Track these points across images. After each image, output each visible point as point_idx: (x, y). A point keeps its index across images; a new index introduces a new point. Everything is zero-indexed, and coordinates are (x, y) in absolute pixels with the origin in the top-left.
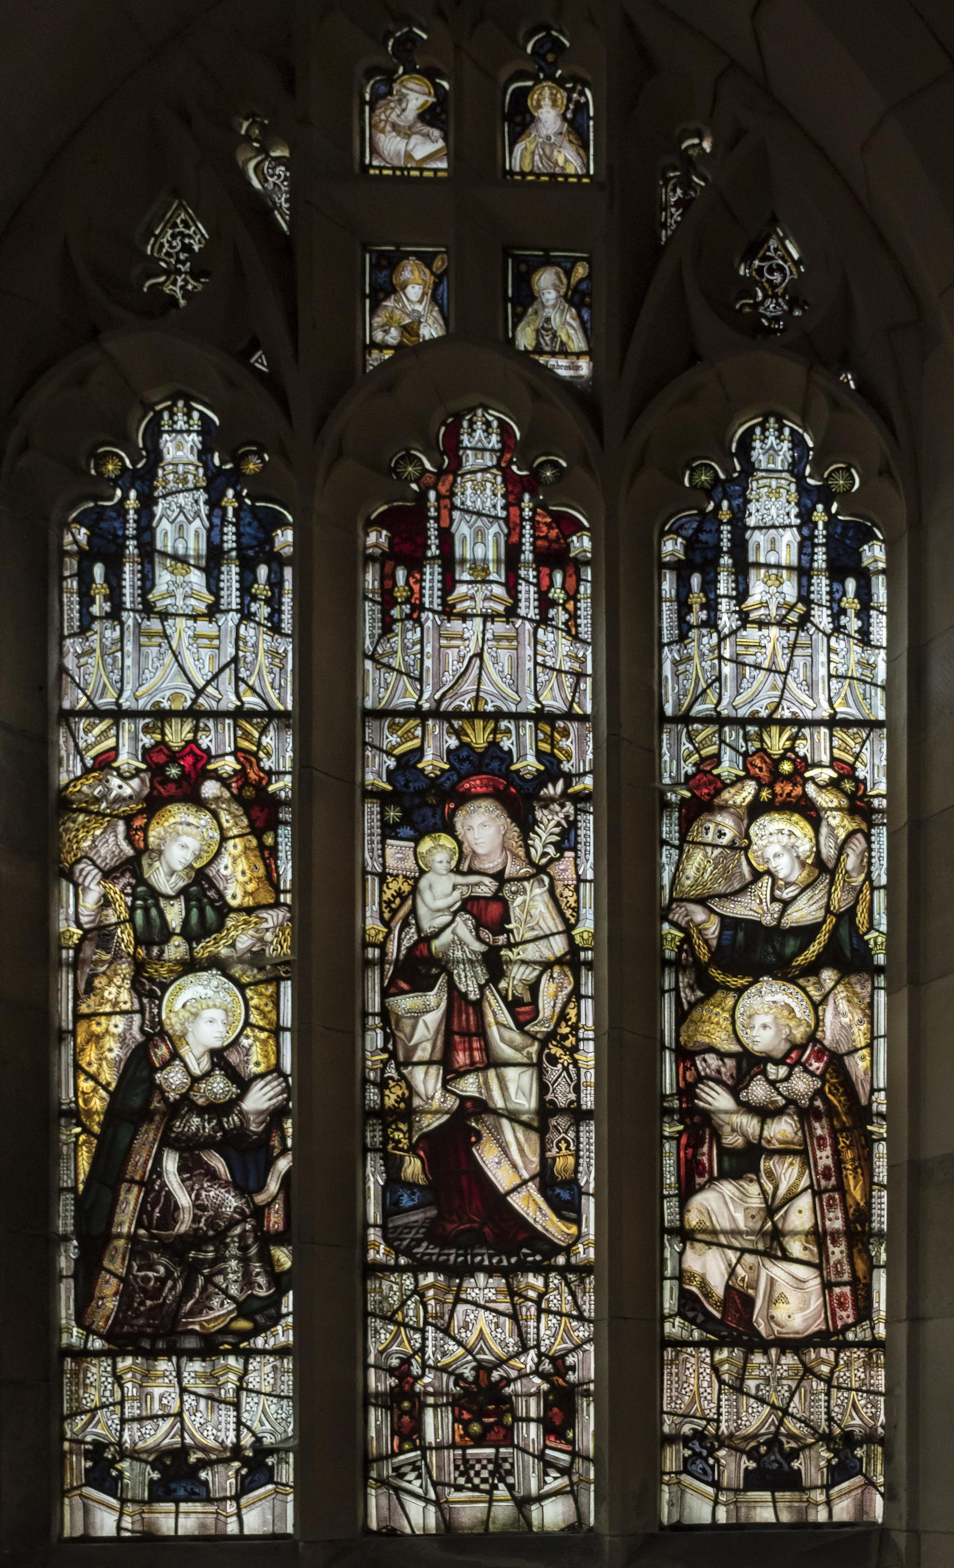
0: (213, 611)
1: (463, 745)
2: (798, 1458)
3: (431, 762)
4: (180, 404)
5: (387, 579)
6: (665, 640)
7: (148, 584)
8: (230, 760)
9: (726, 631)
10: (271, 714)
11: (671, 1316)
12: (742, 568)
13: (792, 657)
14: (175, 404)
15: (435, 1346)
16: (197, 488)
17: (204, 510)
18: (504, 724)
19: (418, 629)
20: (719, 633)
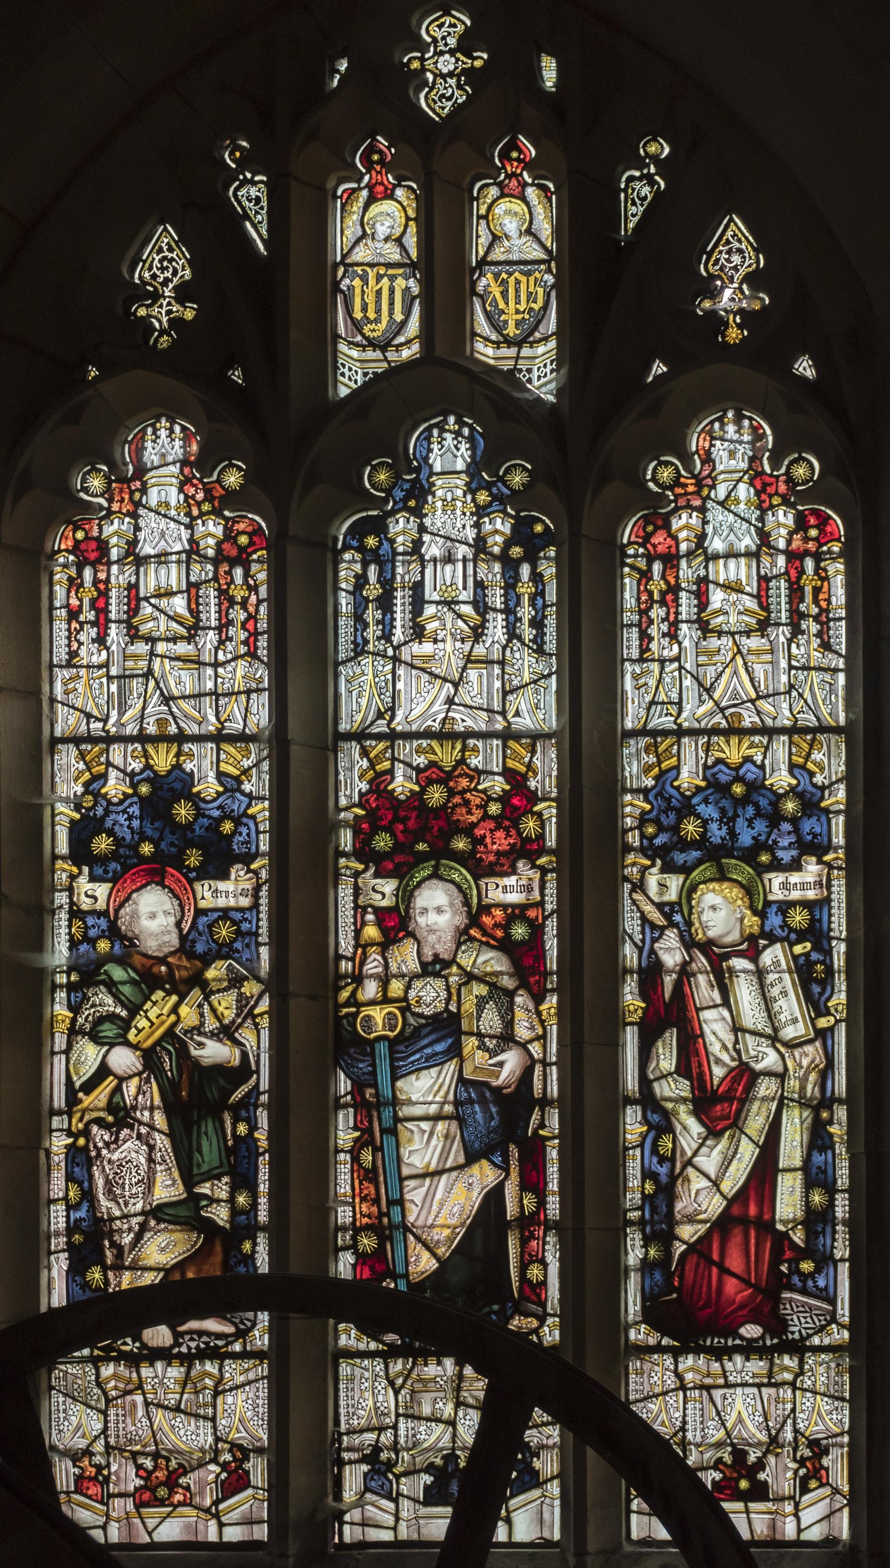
0: (763, 626)
4: (730, 414)
7: (704, 599)
10: (823, 729)
11: (636, 1323)
14: (724, 415)
18: (471, 742)
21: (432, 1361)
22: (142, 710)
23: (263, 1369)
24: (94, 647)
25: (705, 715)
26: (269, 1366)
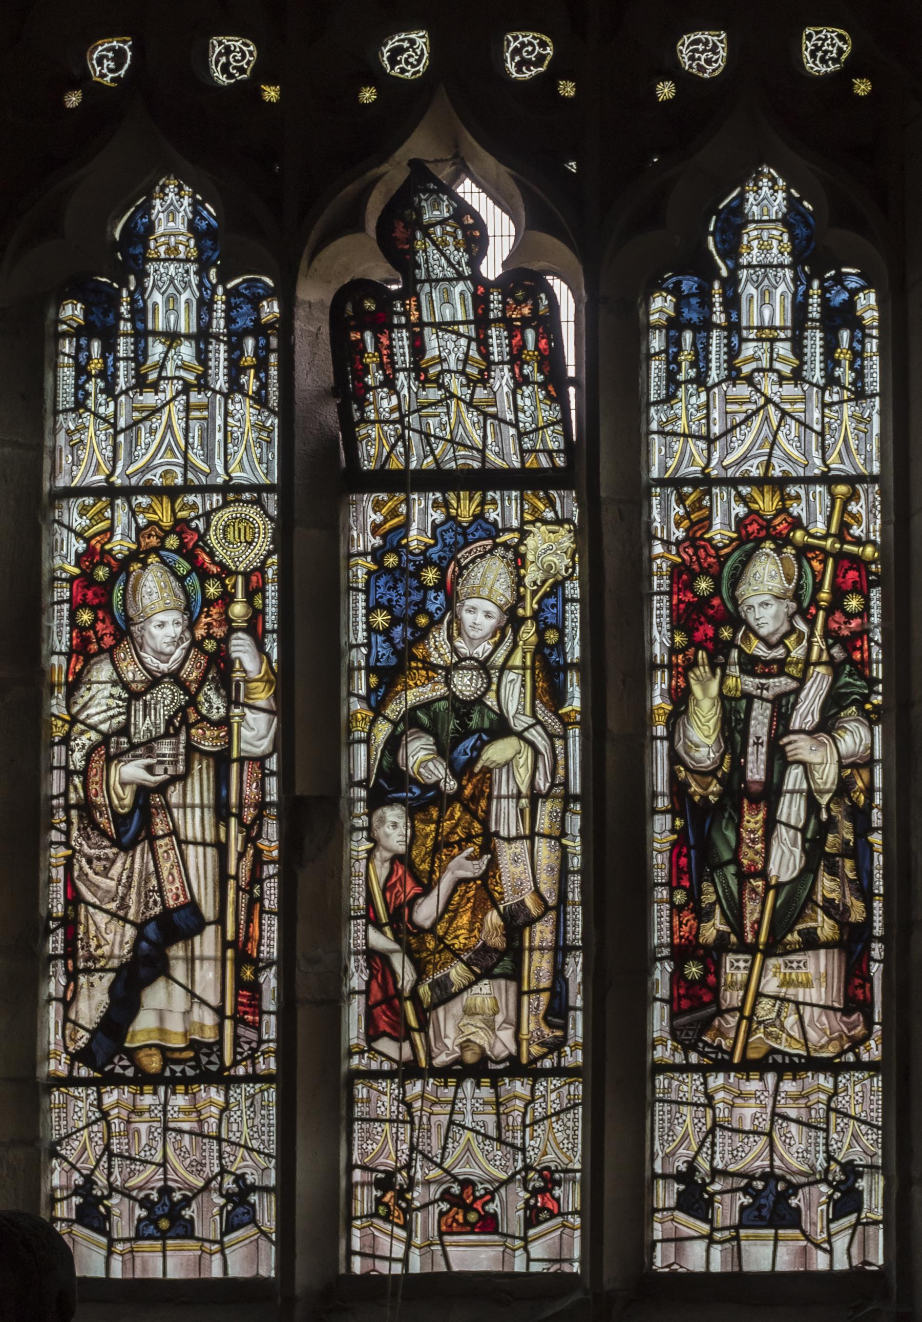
1: (751, 512)
2: (189, 1206)
3: (720, 532)
5: (675, 342)
6: (652, 399)
13: (766, 414)
16: (187, 260)
17: (194, 280)
18: (792, 490)
19: (112, 404)
23: (577, 1089)
25: (134, 473)
26: (277, 1090)
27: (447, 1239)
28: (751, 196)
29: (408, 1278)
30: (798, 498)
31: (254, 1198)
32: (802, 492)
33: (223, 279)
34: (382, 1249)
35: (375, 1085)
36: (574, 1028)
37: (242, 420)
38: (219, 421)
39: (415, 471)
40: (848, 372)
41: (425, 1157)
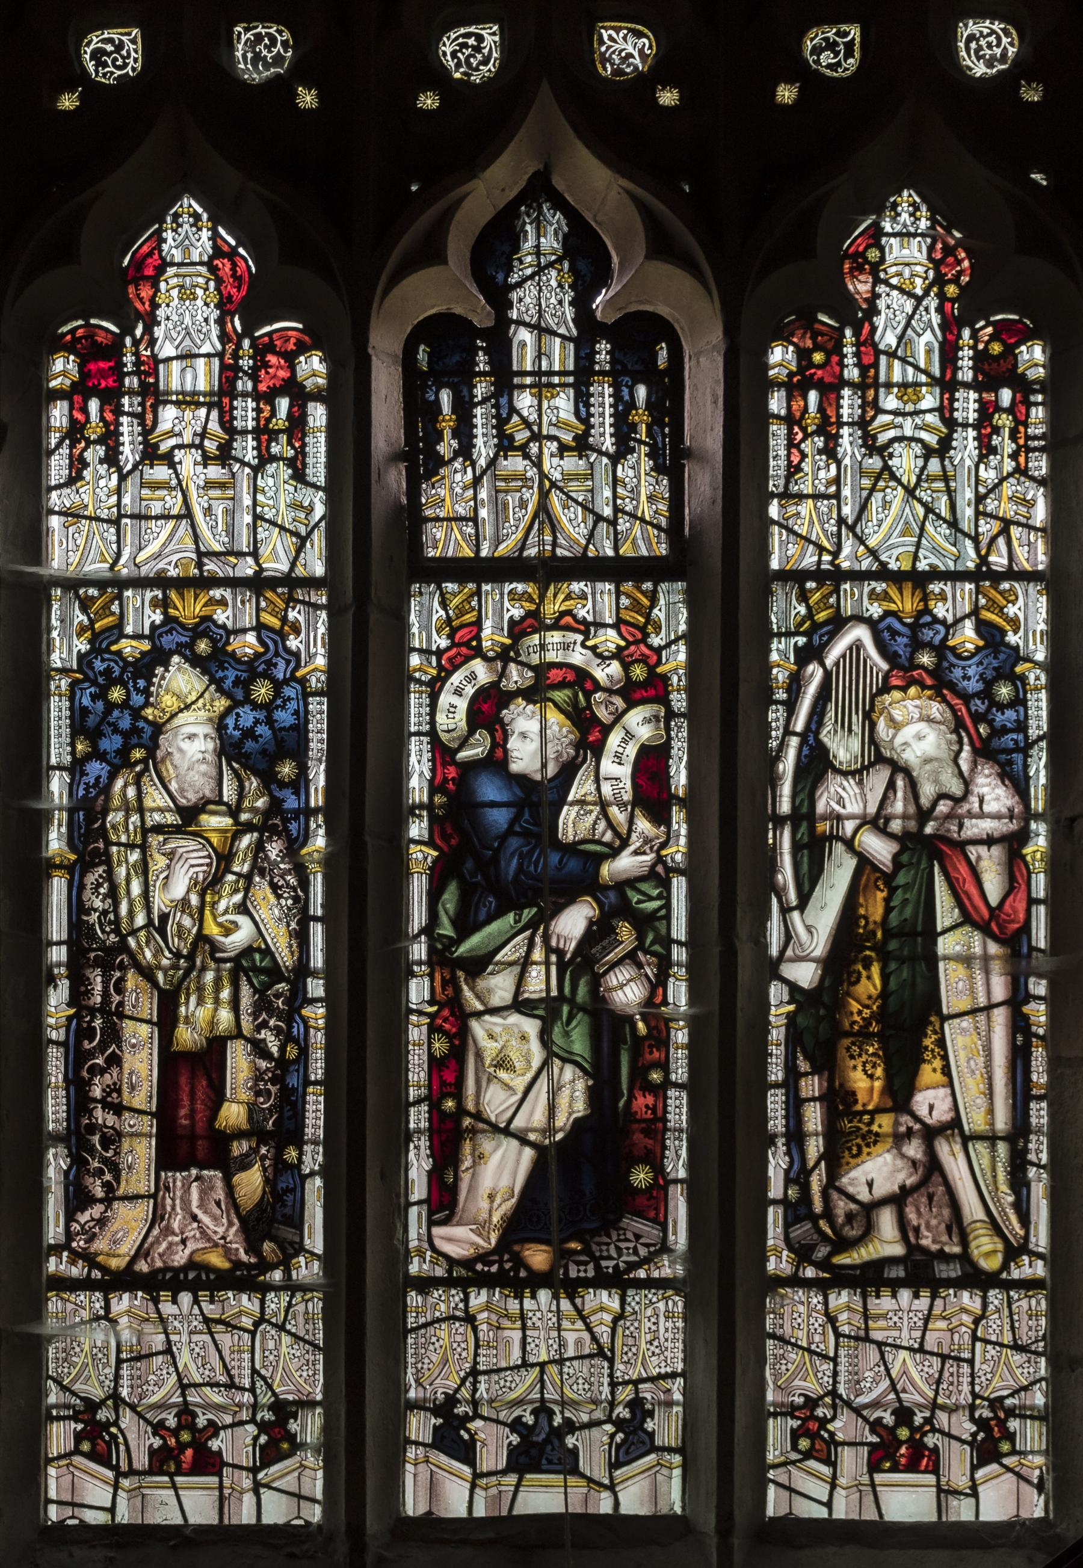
8: (611, 633)
9: (129, 467)
12: (505, 380)
15: (132, 1387)
18: (935, 587)
20: (119, 470)
21: (886, 1292)
22: (162, 548)
24: (102, 469)
25: (147, 561)
27: (879, 1478)
28: (169, 235)
29: (829, 1524)
30: (942, 597)
31: (1014, 1424)
32: (948, 589)
33: (248, 330)
34: (442, 1490)
35: (72, 1298)
36: (675, 1233)
37: (635, 492)
38: (247, 501)
39: (486, 559)
40: (1007, 441)
41: (217, 1385)
